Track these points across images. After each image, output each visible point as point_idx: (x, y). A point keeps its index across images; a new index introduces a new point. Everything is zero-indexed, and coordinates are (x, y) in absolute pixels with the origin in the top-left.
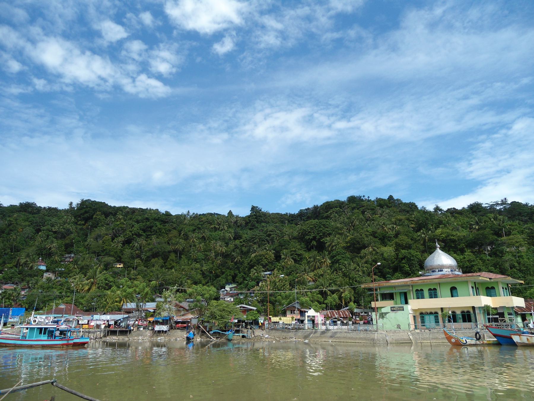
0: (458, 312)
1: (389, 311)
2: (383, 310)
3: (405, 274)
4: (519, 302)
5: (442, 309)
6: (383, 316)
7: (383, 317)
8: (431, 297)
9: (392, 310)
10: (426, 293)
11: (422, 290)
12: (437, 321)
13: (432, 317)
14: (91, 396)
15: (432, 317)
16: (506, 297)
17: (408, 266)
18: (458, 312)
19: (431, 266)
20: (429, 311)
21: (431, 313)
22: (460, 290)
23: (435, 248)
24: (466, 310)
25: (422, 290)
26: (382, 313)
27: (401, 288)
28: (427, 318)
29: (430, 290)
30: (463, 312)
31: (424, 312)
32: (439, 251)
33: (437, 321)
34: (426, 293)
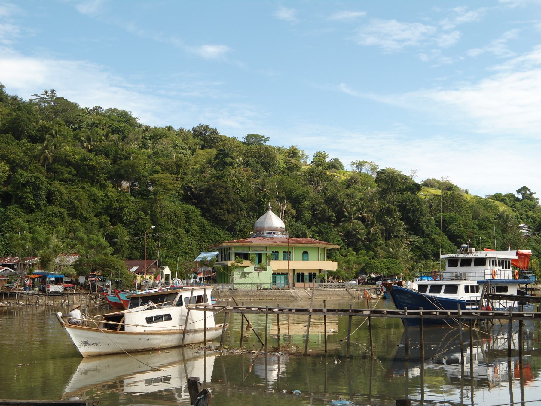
0: (306, 274)
1: (253, 270)
2: (246, 270)
3: (27, 208)
4: (332, 266)
5: (320, 271)
6: (244, 275)
7: (245, 277)
8: (285, 259)
9: (255, 270)
10: (281, 255)
11: (277, 252)
12: (287, 281)
13: (283, 278)
14: (46, 399)
15: (283, 278)
16: (322, 262)
17: (32, 197)
18: (306, 274)
19: (261, 227)
20: (281, 272)
21: (283, 274)
22: (311, 254)
23: (268, 209)
24: (312, 272)
25: (277, 252)
26: (245, 273)
27: (256, 249)
28: (278, 277)
29: (284, 252)
30: (310, 274)
31: (276, 272)
32: (270, 212)
33: (287, 281)
34: (281, 255)
